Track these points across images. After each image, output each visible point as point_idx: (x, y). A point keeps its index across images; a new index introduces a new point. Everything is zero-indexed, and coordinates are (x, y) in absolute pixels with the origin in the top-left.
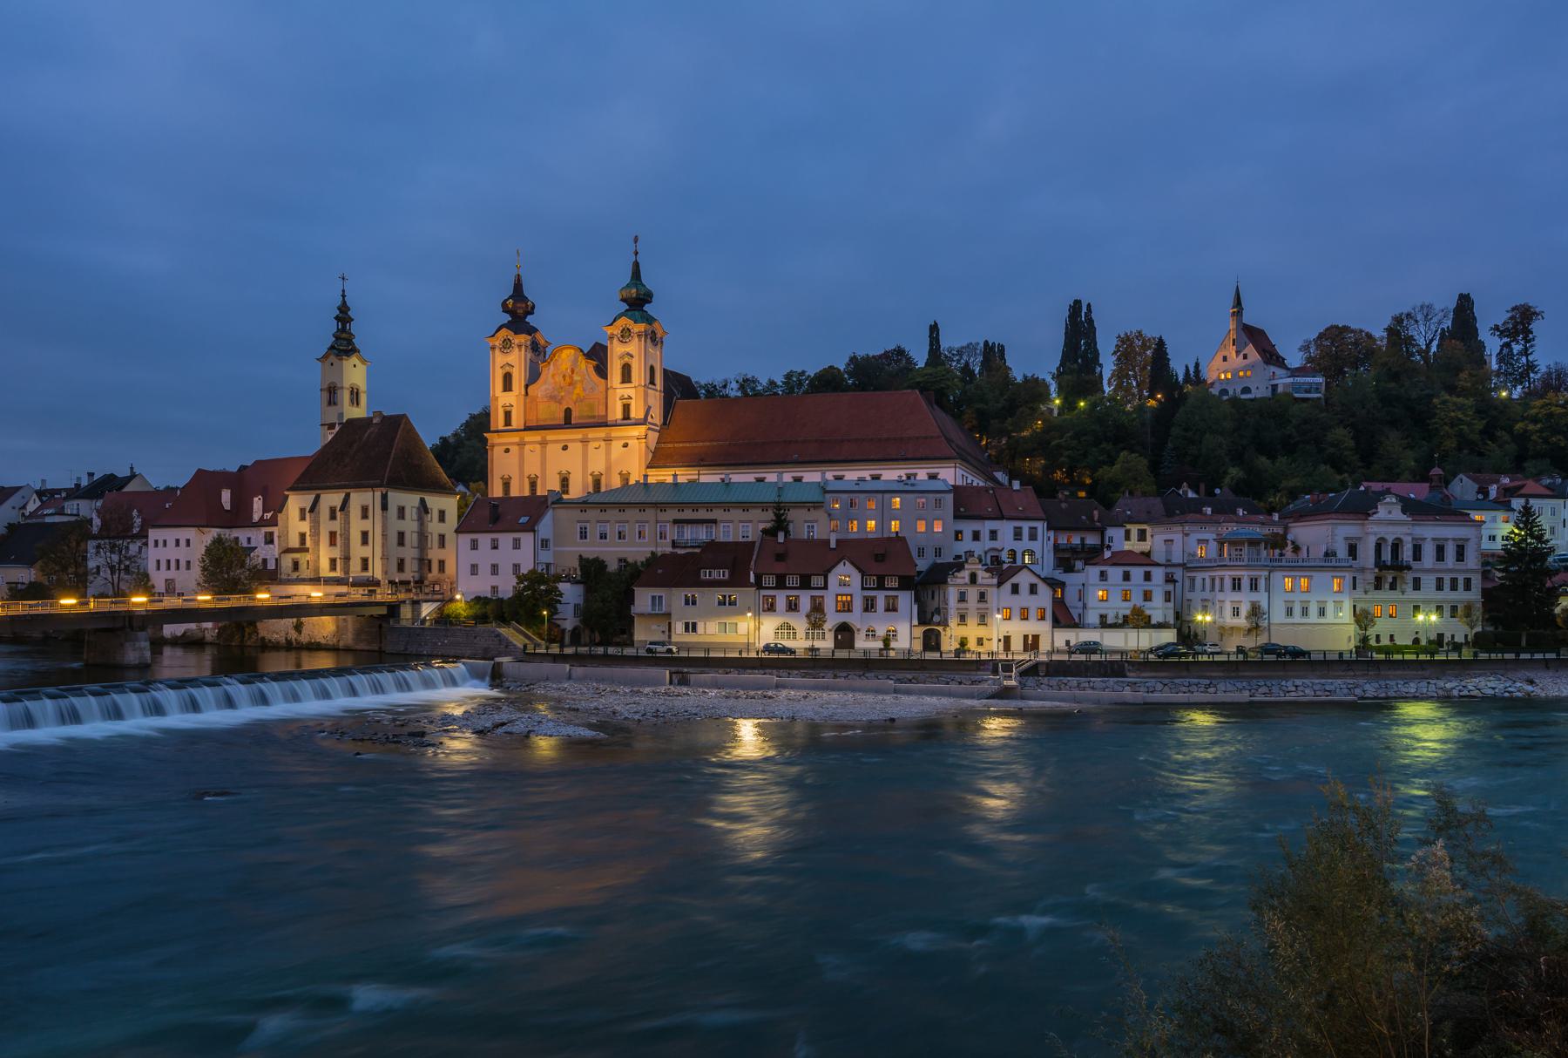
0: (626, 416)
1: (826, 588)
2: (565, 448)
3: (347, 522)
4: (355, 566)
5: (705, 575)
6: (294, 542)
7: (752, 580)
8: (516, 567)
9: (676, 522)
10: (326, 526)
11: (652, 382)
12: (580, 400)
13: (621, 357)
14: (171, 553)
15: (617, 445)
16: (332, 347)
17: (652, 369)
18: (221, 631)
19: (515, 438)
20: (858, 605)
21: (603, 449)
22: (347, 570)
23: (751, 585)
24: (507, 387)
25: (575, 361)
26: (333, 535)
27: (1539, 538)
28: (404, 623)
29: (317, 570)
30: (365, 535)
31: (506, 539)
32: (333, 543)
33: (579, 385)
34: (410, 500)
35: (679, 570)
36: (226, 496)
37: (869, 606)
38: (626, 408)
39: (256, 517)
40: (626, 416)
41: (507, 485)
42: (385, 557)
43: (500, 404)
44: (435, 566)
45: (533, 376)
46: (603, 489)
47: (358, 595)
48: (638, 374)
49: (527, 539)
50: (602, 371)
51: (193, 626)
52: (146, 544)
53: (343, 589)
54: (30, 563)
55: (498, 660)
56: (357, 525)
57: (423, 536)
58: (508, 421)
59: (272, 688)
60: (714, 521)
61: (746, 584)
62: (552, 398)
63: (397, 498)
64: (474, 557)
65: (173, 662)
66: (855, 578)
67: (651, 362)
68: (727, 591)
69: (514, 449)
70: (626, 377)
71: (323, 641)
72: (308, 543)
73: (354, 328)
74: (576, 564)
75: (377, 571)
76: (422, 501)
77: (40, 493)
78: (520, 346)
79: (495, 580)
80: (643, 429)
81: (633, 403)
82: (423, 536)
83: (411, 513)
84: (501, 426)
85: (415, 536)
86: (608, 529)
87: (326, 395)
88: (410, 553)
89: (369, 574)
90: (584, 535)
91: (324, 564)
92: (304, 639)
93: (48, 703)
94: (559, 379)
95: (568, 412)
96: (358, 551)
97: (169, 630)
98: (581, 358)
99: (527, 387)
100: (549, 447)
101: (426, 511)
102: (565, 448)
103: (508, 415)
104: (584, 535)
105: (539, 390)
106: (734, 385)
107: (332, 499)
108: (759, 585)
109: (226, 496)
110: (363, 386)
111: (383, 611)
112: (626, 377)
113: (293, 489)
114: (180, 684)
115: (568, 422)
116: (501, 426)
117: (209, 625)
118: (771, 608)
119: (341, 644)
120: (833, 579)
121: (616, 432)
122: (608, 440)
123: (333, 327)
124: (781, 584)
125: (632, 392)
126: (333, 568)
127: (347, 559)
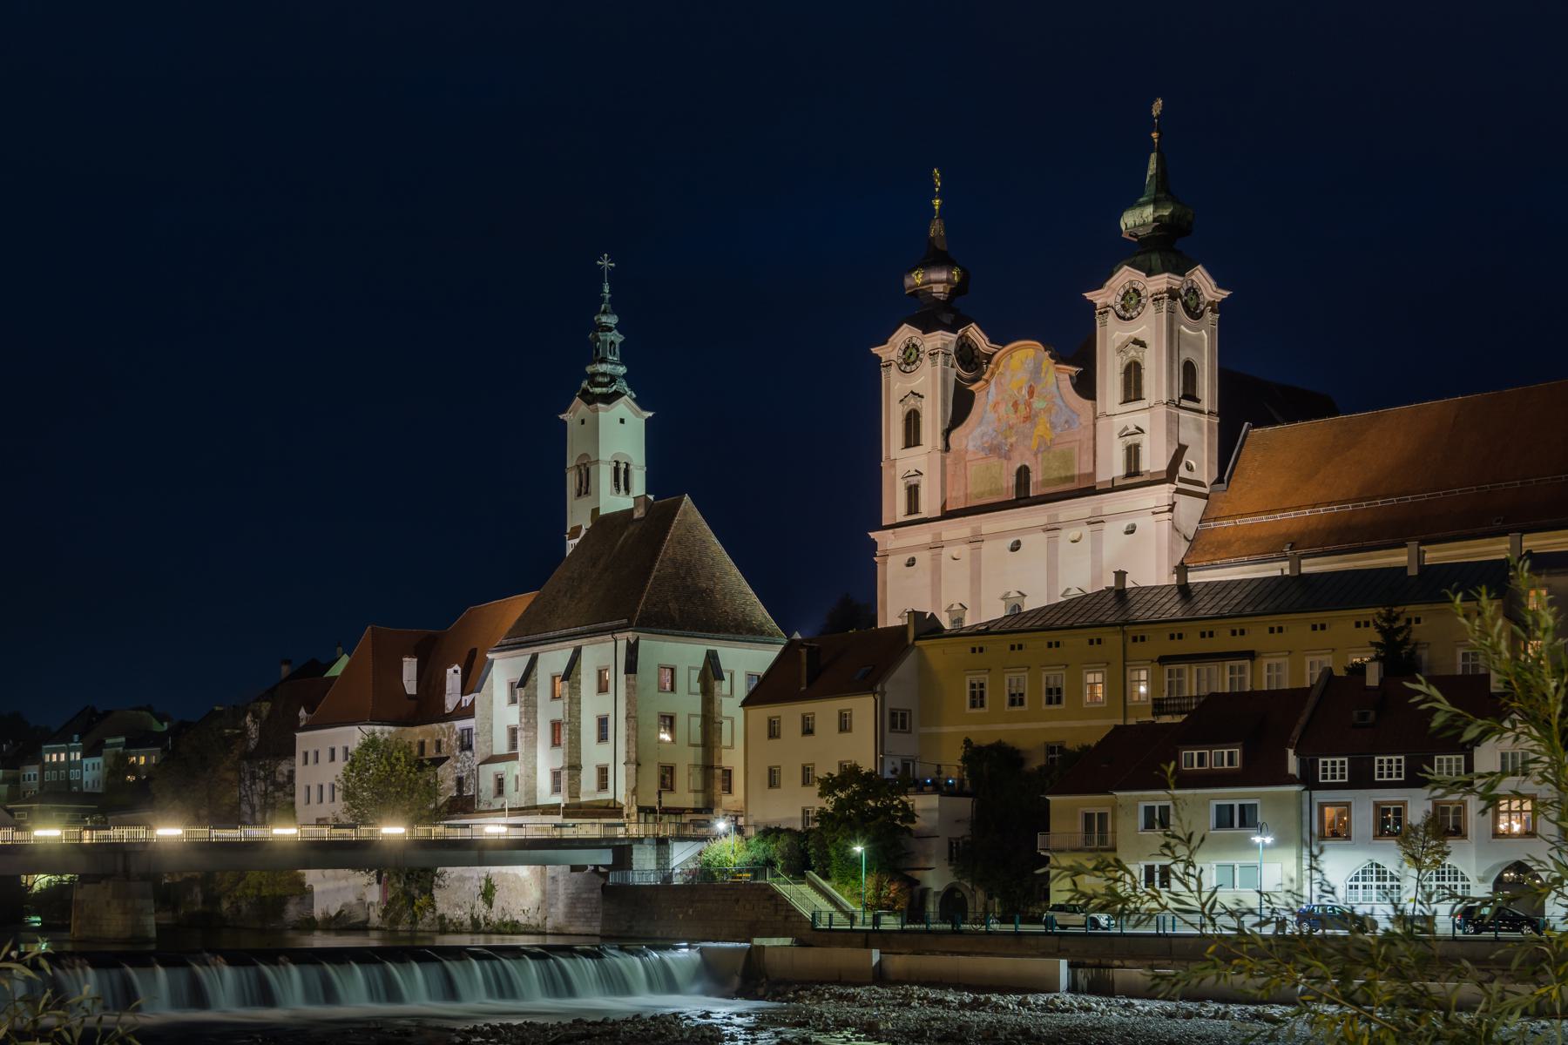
0: (1133, 470)
2: (1016, 547)
3: (575, 701)
4: (588, 779)
5: (1191, 758)
6: (501, 747)
7: (1293, 766)
9: (1164, 660)
10: (549, 711)
11: (1190, 394)
12: (1045, 447)
13: (1122, 349)
15: (1113, 531)
19: (923, 535)
21: (1086, 543)
22: (574, 791)
23: (1291, 780)
24: (912, 437)
25: (1037, 371)
26: (556, 726)
28: (636, 879)
29: (532, 791)
30: (603, 722)
31: (826, 711)
32: (555, 743)
33: (1043, 419)
34: (688, 653)
35: (1131, 758)
36: (410, 667)
38: (1133, 453)
39: (450, 705)
40: (1133, 470)
42: (637, 763)
45: (961, 406)
47: (589, 829)
48: (1157, 381)
49: (863, 708)
50: (1086, 386)
53: (559, 819)
54: (785, 936)
55: (757, 941)
56: (593, 705)
58: (913, 506)
60: (1251, 655)
62: (994, 450)
63: (661, 650)
64: (772, 753)
67: (1186, 354)
69: (923, 558)
71: (522, 920)
72: (520, 749)
75: (620, 790)
76: (712, 658)
80: (1164, 493)
81: (1145, 441)
83: (689, 681)
85: (697, 722)
89: (607, 796)
90: (977, 699)
91: (544, 782)
92: (495, 916)
95: (1023, 474)
96: (594, 754)
99: (947, 434)
100: (986, 547)
102: (1016, 547)
103: (913, 492)
104: (977, 699)
105: (969, 436)
107: (554, 659)
108: (1309, 779)
109: (410, 667)
111: (606, 858)
113: (502, 648)
115: (1023, 497)
116: (901, 514)
118: (1340, 833)
119: (549, 924)
121: (1110, 503)
122: (1096, 521)
124: (1361, 779)
125: (1142, 419)
126: (556, 789)
127: (575, 767)
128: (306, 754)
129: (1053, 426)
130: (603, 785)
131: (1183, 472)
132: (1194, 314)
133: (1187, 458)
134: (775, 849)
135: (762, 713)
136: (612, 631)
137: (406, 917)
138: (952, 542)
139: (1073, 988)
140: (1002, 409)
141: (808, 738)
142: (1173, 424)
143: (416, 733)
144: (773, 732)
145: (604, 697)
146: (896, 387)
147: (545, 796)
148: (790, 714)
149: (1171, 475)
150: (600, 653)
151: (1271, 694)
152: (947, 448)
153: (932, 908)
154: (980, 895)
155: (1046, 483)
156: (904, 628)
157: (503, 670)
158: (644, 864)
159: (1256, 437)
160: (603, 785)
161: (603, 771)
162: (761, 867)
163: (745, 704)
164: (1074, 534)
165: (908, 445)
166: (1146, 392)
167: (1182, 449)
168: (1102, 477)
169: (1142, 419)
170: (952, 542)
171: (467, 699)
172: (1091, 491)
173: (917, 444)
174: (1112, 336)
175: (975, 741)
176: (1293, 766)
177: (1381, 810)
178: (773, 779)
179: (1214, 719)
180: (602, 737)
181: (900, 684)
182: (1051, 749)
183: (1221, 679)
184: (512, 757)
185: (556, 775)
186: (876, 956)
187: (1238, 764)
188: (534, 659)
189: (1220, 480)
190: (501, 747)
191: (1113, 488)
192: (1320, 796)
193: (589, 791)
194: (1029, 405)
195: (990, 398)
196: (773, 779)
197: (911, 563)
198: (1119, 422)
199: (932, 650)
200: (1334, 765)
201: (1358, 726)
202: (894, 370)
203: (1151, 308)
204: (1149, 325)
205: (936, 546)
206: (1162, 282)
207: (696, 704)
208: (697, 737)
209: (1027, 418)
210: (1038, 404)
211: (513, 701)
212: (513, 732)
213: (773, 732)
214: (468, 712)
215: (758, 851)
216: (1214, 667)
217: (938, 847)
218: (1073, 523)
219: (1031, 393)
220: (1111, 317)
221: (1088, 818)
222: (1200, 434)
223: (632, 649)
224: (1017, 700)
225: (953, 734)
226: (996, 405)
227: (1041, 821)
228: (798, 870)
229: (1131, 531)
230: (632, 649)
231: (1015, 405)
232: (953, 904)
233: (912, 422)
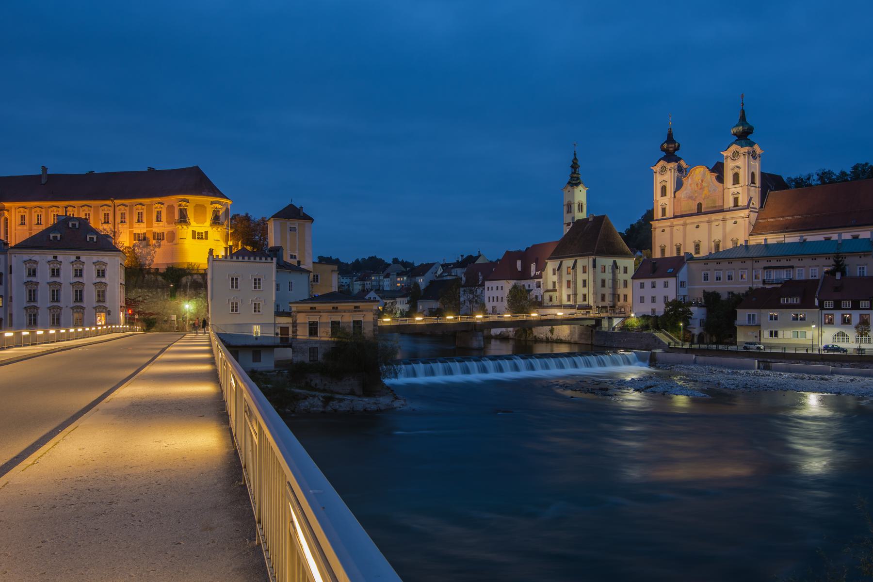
5: (784, 301)
6: (550, 287)
7: (817, 303)
8: (666, 298)
9: (765, 268)
11: (753, 182)
13: (733, 169)
15: (730, 224)
18: (517, 332)
21: (721, 227)
22: (575, 301)
23: (816, 307)
25: (704, 175)
26: (569, 282)
28: (604, 329)
29: (561, 300)
31: (659, 282)
32: (569, 287)
34: (608, 262)
35: (767, 298)
36: (519, 263)
38: (736, 200)
39: (532, 274)
41: (663, 251)
42: (595, 294)
43: (659, 204)
44: (622, 298)
45: (679, 185)
46: (721, 250)
47: (580, 314)
48: (744, 178)
49: (672, 281)
50: (720, 179)
51: (504, 330)
53: (573, 311)
56: (581, 277)
58: (664, 214)
59: (537, 362)
60: (792, 267)
62: (690, 198)
65: (496, 348)
69: (667, 230)
70: (736, 179)
74: (701, 296)
75: (591, 301)
76: (615, 262)
77: (443, 266)
78: (671, 169)
79: (653, 306)
80: (747, 212)
81: (740, 196)
82: (614, 281)
83: (609, 269)
84: (660, 217)
91: (565, 298)
92: (554, 337)
93: (421, 365)
94: (694, 186)
95: (700, 205)
96: (581, 291)
97: (495, 331)
99: (675, 192)
102: (698, 227)
103: (664, 210)
105: (682, 194)
106: (815, 177)
107: (568, 263)
108: (821, 307)
109: (519, 263)
110: (584, 202)
111: (593, 323)
112: (736, 179)
113: (550, 259)
114: (568, 355)
115: (699, 212)
116: (660, 217)
117: (511, 329)
118: (831, 322)
121: (728, 215)
123: (569, 171)
124: (837, 307)
125: (739, 190)
126: (569, 300)
127: (575, 295)
130: (585, 299)
131: (751, 205)
132: (754, 157)
133: (752, 201)
134: (650, 322)
135: (638, 282)
136: (588, 255)
137: (524, 336)
138: (677, 225)
139: (759, 368)
142: (749, 190)
143: (523, 282)
144: (642, 286)
146: (658, 179)
147: (565, 302)
148: (648, 282)
149: (748, 207)
150: (582, 262)
151: (806, 281)
153: (696, 340)
154: (708, 336)
155: (707, 208)
157: (551, 265)
158: (605, 323)
159: (772, 194)
160: (585, 299)
161: (585, 296)
162: (646, 327)
163: (633, 278)
164: (717, 223)
165: (662, 196)
167: (751, 198)
168: (726, 207)
169: (739, 190)
170: (677, 225)
171: (538, 273)
172: (722, 211)
174: (730, 166)
175: (707, 291)
176: (817, 303)
178: (642, 300)
179: (791, 287)
180: (584, 286)
181: (683, 274)
182: (729, 293)
183: (783, 275)
184: (554, 290)
185: (569, 296)
186: (694, 356)
187: (799, 302)
188: (561, 262)
189: (761, 207)
190: (550, 287)
191: (729, 210)
192: (824, 312)
193: (580, 300)
195: (689, 183)
196: (642, 300)
197: (663, 231)
198: (732, 191)
199: (694, 266)
200: (829, 304)
201: (836, 291)
202: (658, 174)
203: (742, 157)
204: (741, 162)
205: (672, 226)
206: (746, 149)
207: (610, 276)
208: (611, 286)
210: (704, 184)
211: (554, 274)
212: (554, 283)
213: (642, 286)
214: (540, 277)
215: (643, 322)
216: (782, 270)
217: (697, 322)
218: (716, 220)
220: (729, 160)
221: (749, 316)
222: (756, 193)
223: (594, 261)
224: (718, 279)
225: (697, 290)
227: (734, 316)
228: (658, 328)
229: (735, 223)
230: (594, 261)
232: (701, 339)
233: (664, 189)
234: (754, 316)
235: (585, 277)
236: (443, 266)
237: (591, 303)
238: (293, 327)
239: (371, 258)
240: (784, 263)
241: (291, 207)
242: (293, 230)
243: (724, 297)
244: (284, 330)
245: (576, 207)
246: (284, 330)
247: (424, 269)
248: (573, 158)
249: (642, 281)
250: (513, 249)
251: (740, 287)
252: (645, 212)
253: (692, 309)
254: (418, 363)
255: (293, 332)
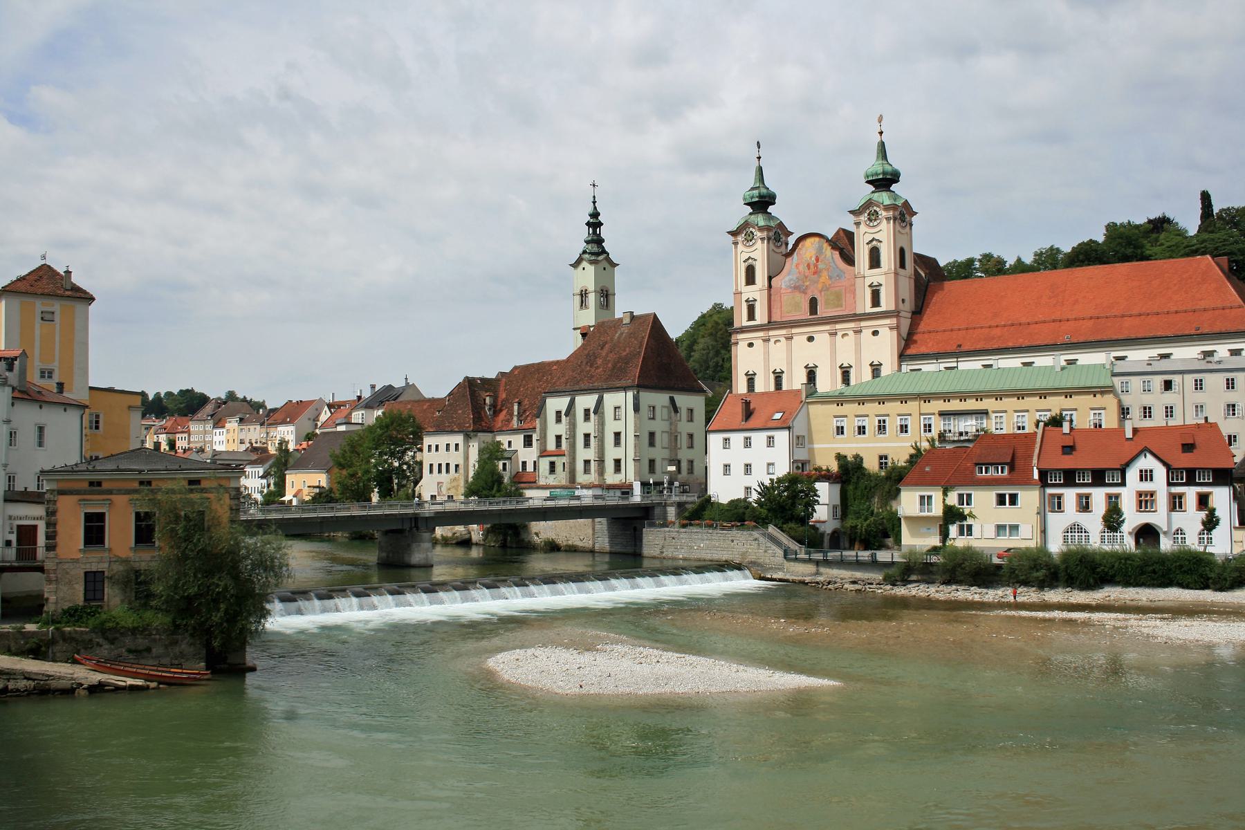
1: (1123, 484)
7: (1036, 476)
11: (902, 265)
12: (826, 288)
14: (441, 457)
16: (584, 252)
17: (902, 251)
20: (1162, 501)
22: (601, 472)
25: (820, 249)
27: (764, 535)
31: (759, 438)
33: (825, 274)
37: (1176, 503)
49: (782, 437)
50: (849, 260)
52: (421, 450)
56: (611, 427)
57: (674, 437)
61: (1026, 482)
66: (1160, 472)
68: (1007, 491)
70: (875, 261)
73: (604, 232)
76: (672, 400)
77: (330, 406)
82: (674, 437)
83: (661, 413)
84: (745, 323)
85: (665, 436)
86: (866, 422)
87: (578, 298)
88: (659, 453)
96: (612, 453)
98: (826, 245)
99: (770, 278)
101: (676, 410)
107: (586, 401)
110: (591, 288)
112: (875, 261)
120: (1132, 475)
123: (585, 232)
125: (882, 280)
127: (601, 461)
128: (431, 465)
129: (830, 278)
140: (801, 268)
141: (748, 462)
145: (1168, 394)
152: (770, 286)
156: (799, 391)
161: (617, 462)
166: (882, 264)
173: (586, 307)
177: (1080, 496)
183: (969, 426)
187: (1006, 473)
194: (816, 266)
209: (815, 273)
219: (817, 260)
221: (922, 498)
223: (636, 399)
226: (797, 266)
231: (808, 266)
234: (930, 497)
235: (618, 426)
236: (330, 406)
237: (631, 477)
238: (48, 525)
239: (183, 393)
240: (971, 404)
241: (44, 272)
242: (47, 317)
243: (871, 464)
244: (26, 534)
245: (592, 298)
246: (26, 534)
247: (290, 412)
248: (590, 209)
249: (747, 434)
250: (476, 374)
251: (899, 449)
252: (1126, 221)
253: (818, 485)
254: (346, 596)
255: (48, 538)
